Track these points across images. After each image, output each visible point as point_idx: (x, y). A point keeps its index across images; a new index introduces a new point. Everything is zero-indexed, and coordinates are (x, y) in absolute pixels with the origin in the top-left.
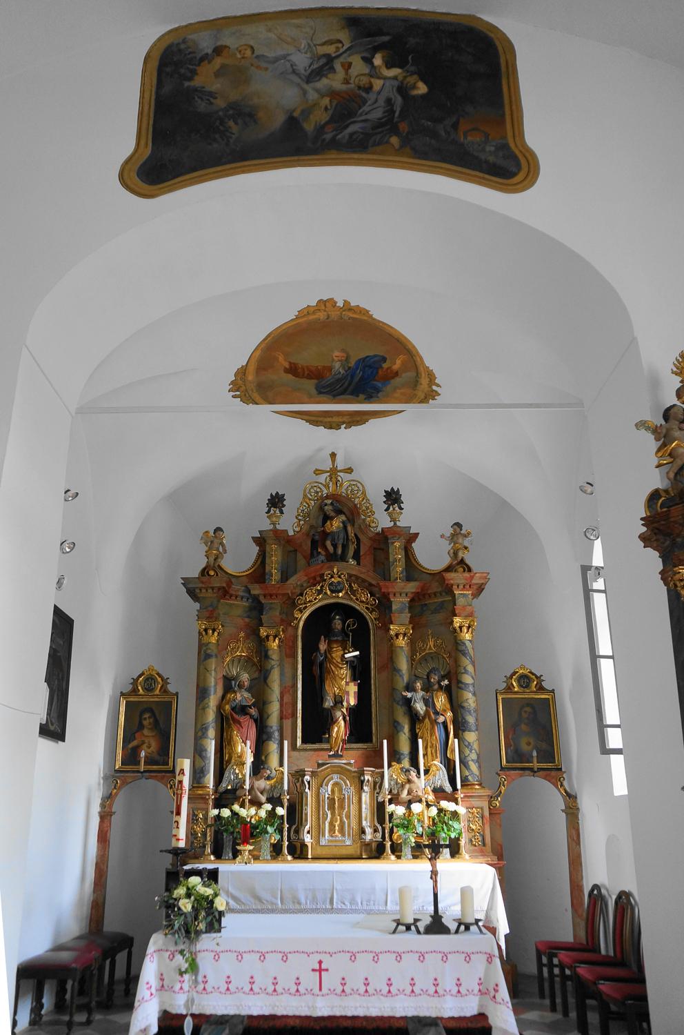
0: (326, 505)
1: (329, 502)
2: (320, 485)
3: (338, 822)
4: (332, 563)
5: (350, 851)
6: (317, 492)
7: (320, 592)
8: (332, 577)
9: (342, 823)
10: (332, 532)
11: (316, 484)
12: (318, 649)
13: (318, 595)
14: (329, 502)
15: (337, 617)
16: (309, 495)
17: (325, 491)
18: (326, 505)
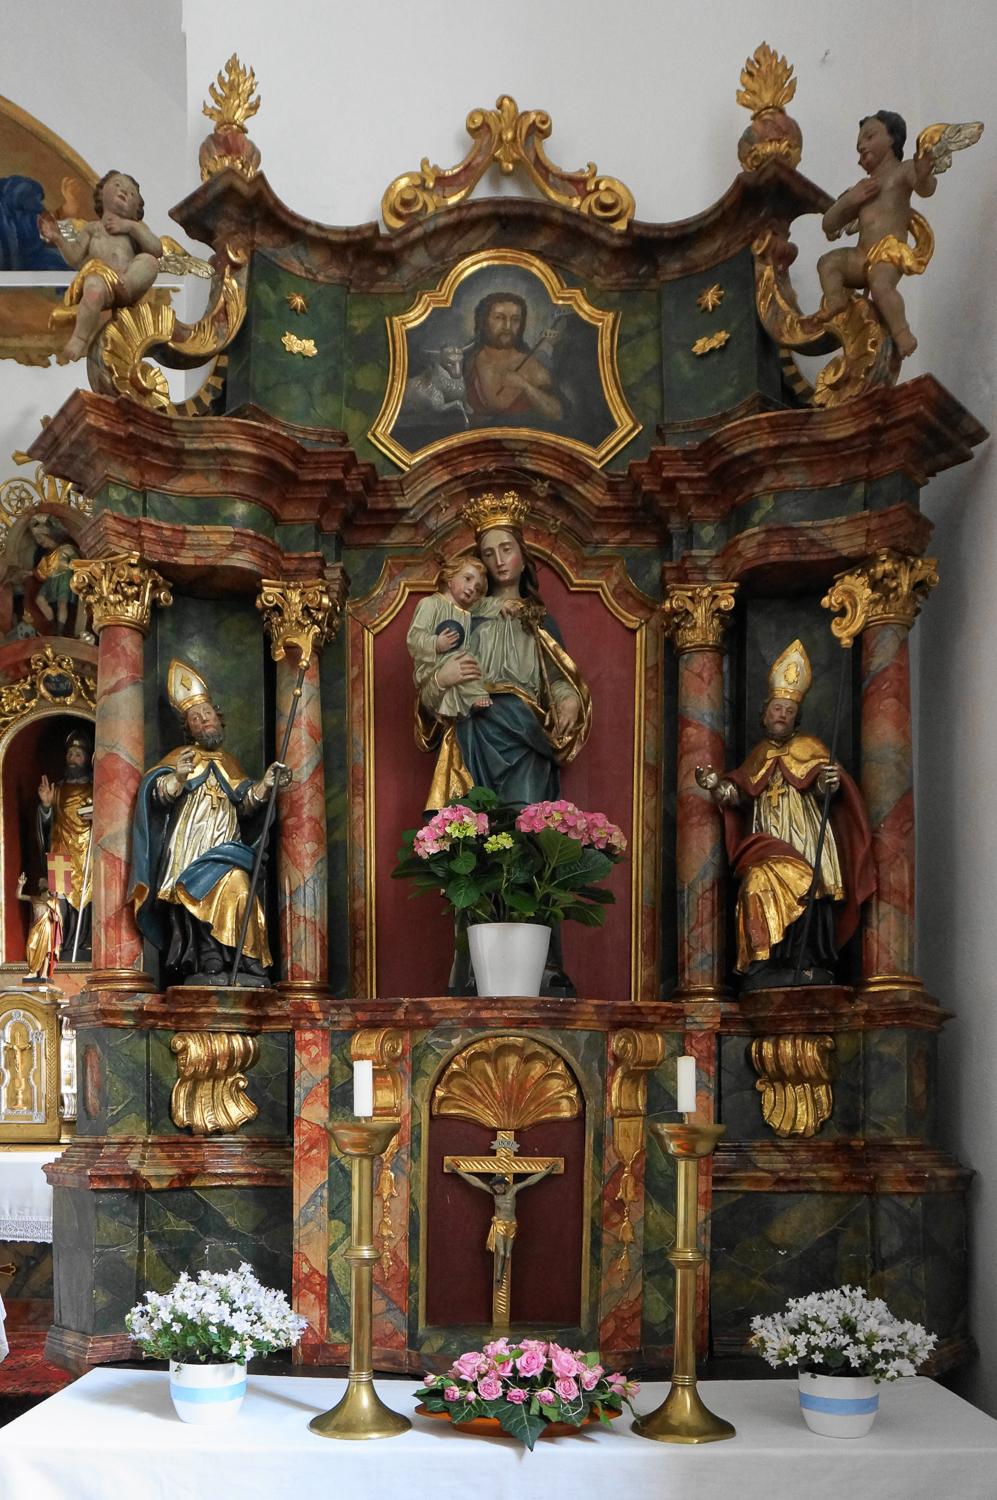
0: (37, 524)
1: (43, 519)
2: (27, 486)
3: (23, 1086)
4: (44, 639)
5: (44, 1133)
6: (21, 500)
7: (32, 693)
8: (46, 666)
9: (29, 1087)
10: (49, 579)
11: (19, 484)
12: (40, 801)
13: (28, 701)
14: (43, 519)
15: (76, 742)
16: (5, 505)
17: (37, 498)
18: (37, 524)
